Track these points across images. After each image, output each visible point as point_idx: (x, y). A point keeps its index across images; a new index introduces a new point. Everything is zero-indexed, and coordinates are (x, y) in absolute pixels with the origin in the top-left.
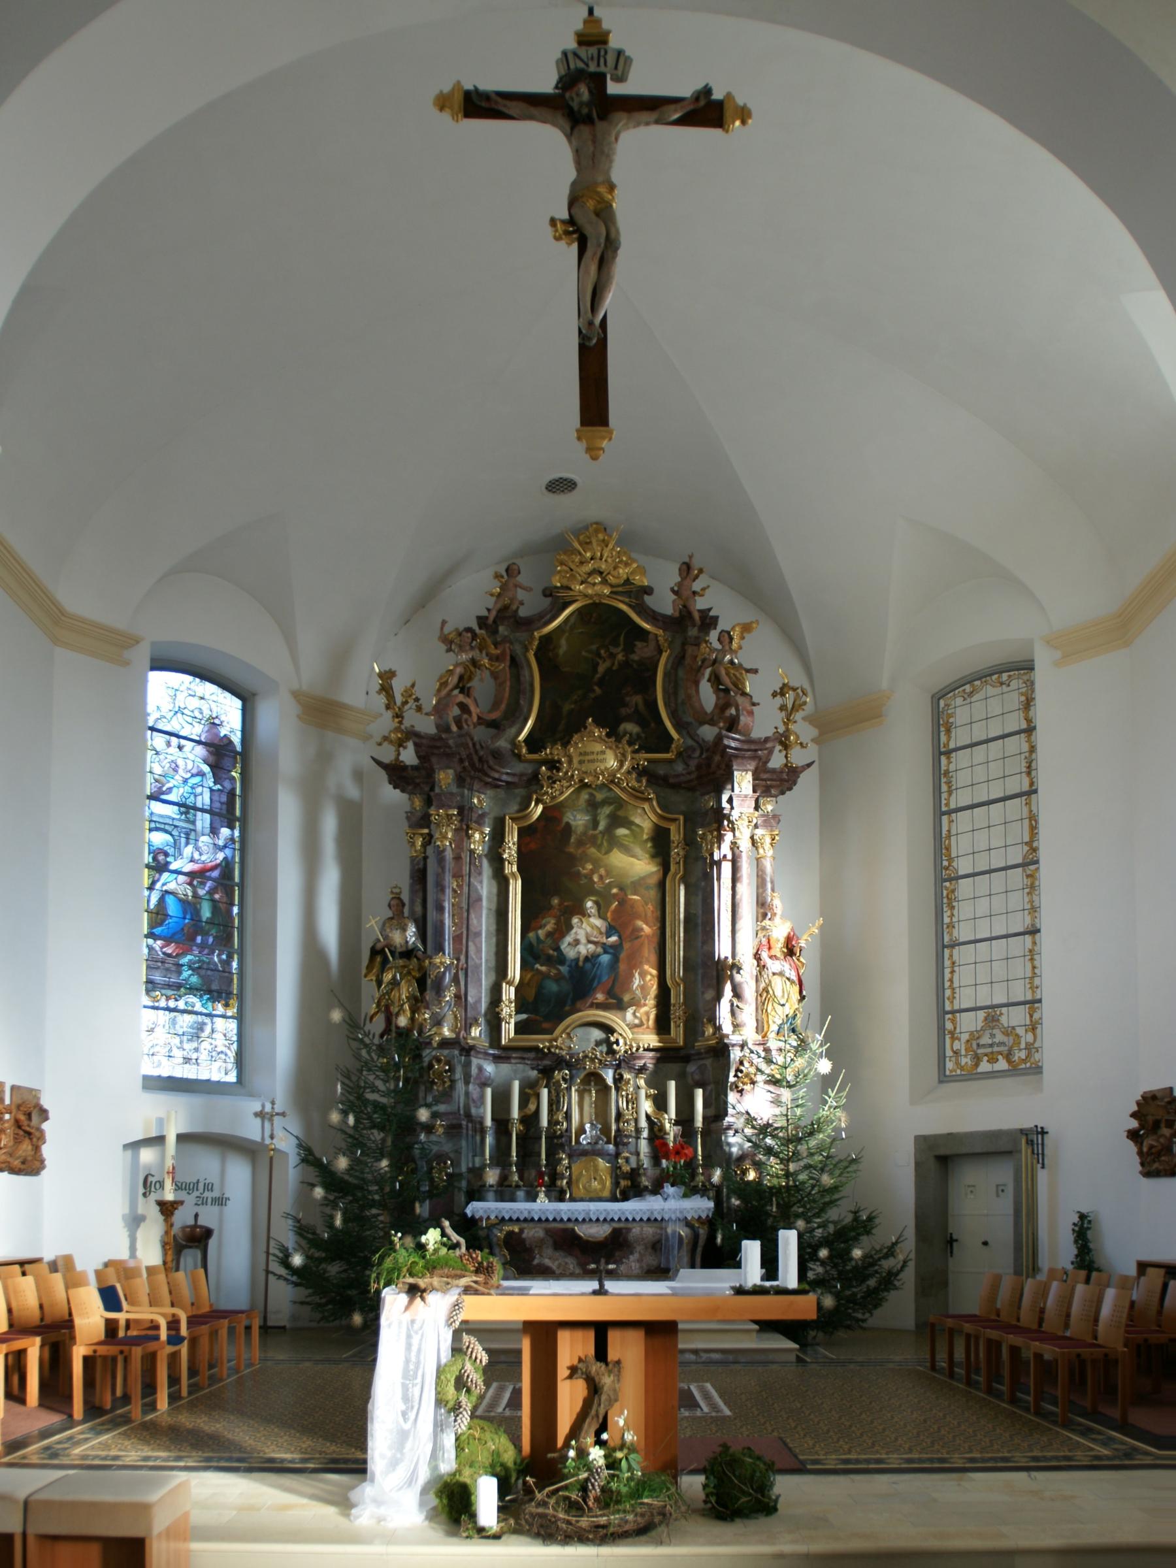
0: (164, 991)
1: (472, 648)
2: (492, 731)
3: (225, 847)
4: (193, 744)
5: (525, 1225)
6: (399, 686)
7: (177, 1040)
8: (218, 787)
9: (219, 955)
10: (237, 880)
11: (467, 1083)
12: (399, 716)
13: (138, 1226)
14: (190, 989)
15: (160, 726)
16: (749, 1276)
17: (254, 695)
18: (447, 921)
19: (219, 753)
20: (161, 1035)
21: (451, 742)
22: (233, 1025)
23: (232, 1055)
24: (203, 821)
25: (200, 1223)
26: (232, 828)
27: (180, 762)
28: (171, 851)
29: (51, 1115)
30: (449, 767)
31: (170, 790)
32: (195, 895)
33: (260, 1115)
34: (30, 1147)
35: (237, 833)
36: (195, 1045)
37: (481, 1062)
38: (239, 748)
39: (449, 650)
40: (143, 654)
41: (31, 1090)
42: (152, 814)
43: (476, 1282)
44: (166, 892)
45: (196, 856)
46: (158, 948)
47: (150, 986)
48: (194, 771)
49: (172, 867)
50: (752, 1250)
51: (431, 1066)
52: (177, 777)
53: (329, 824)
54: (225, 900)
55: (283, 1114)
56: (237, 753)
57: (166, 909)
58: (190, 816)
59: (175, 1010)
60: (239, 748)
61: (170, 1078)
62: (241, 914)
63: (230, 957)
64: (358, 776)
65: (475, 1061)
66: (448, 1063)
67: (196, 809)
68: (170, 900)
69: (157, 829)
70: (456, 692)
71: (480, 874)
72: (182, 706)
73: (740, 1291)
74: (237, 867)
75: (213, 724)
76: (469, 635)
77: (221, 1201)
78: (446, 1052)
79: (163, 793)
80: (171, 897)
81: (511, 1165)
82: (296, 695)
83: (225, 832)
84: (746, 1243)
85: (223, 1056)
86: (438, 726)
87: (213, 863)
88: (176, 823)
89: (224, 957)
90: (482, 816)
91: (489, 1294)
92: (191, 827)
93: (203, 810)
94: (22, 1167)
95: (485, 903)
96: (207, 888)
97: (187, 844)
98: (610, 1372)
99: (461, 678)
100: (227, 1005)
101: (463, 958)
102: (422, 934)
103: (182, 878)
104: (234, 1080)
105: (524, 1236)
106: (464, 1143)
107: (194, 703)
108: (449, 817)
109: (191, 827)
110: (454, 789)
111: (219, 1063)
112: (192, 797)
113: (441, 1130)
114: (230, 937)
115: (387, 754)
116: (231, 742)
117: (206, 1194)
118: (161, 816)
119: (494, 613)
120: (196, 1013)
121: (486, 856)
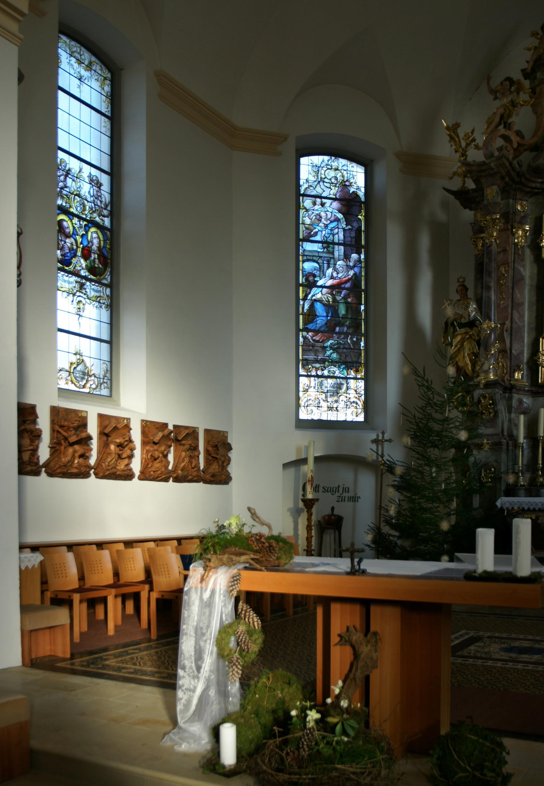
0: (314, 365)
1: (511, 92)
2: (534, 154)
3: (354, 266)
4: (330, 201)
5: (540, 514)
6: (461, 132)
7: (323, 396)
8: (349, 227)
9: (351, 339)
10: (363, 287)
11: (510, 412)
12: (464, 155)
13: (299, 515)
14: (332, 362)
15: (309, 192)
16: (479, 561)
17: (372, 161)
18: (493, 298)
19: (348, 203)
20: (312, 393)
21: (492, 165)
22: (362, 384)
23: (360, 403)
24: (339, 251)
25: (335, 513)
26: (359, 253)
27: (323, 214)
28: (317, 273)
29: (233, 447)
30: (493, 184)
31: (316, 234)
32: (334, 300)
33: (376, 441)
34: (217, 467)
35: (362, 256)
36: (335, 398)
37: (520, 396)
38: (363, 199)
39: (496, 98)
40: (290, 147)
41: (219, 432)
42: (304, 250)
43: (253, 559)
44: (315, 300)
45: (335, 275)
46: (310, 338)
47: (305, 362)
48: (333, 219)
49: (319, 284)
50: (486, 538)
51: (479, 401)
52: (321, 224)
53: (424, 241)
54: (355, 301)
55: (390, 441)
56: (361, 202)
57: (315, 312)
58: (330, 249)
59: (322, 376)
60: (363, 199)
61: (318, 420)
62: (365, 310)
63: (359, 340)
64: (445, 205)
65: (516, 396)
66: (491, 398)
67: (334, 243)
68: (318, 306)
69: (308, 260)
70: (501, 127)
71: (523, 260)
72: (323, 176)
73: (470, 577)
74: (363, 278)
75: (345, 185)
76: (508, 83)
77: (355, 499)
78: (490, 391)
79: (312, 236)
80: (318, 303)
81: (538, 471)
82: (398, 155)
83: (354, 256)
84: (480, 531)
85: (355, 405)
86: (486, 156)
87: (347, 278)
88: (321, 255)
89: (355, 339)
90: (524, 217)
91: (261, 570)
92: (331, 256)
93: (339, 244)
94: (212, 479)
95: (527, 281)
96: (342, 295)
97: (328, 267)
98: (368, 642)
99: (502, 117)
100: (357, 371)
101: (508, 323)
102: (480, 308)
103: (325, 290)
104: (362, 420)
105: (539, 522)
106: (504, 456)
107: (331, 174)
108: (494, 221)
109: (331, 256)
110: (499, 199)
111: (352, 409)
112: (331, 237)
113: (487, 447)
114: (359, 326)
115: (456, 184)
116: (357, 196)
117: (345, 494)
118: (310, 251)
119: (531, 63)
120: (336, 378)
121: (529, 246)
